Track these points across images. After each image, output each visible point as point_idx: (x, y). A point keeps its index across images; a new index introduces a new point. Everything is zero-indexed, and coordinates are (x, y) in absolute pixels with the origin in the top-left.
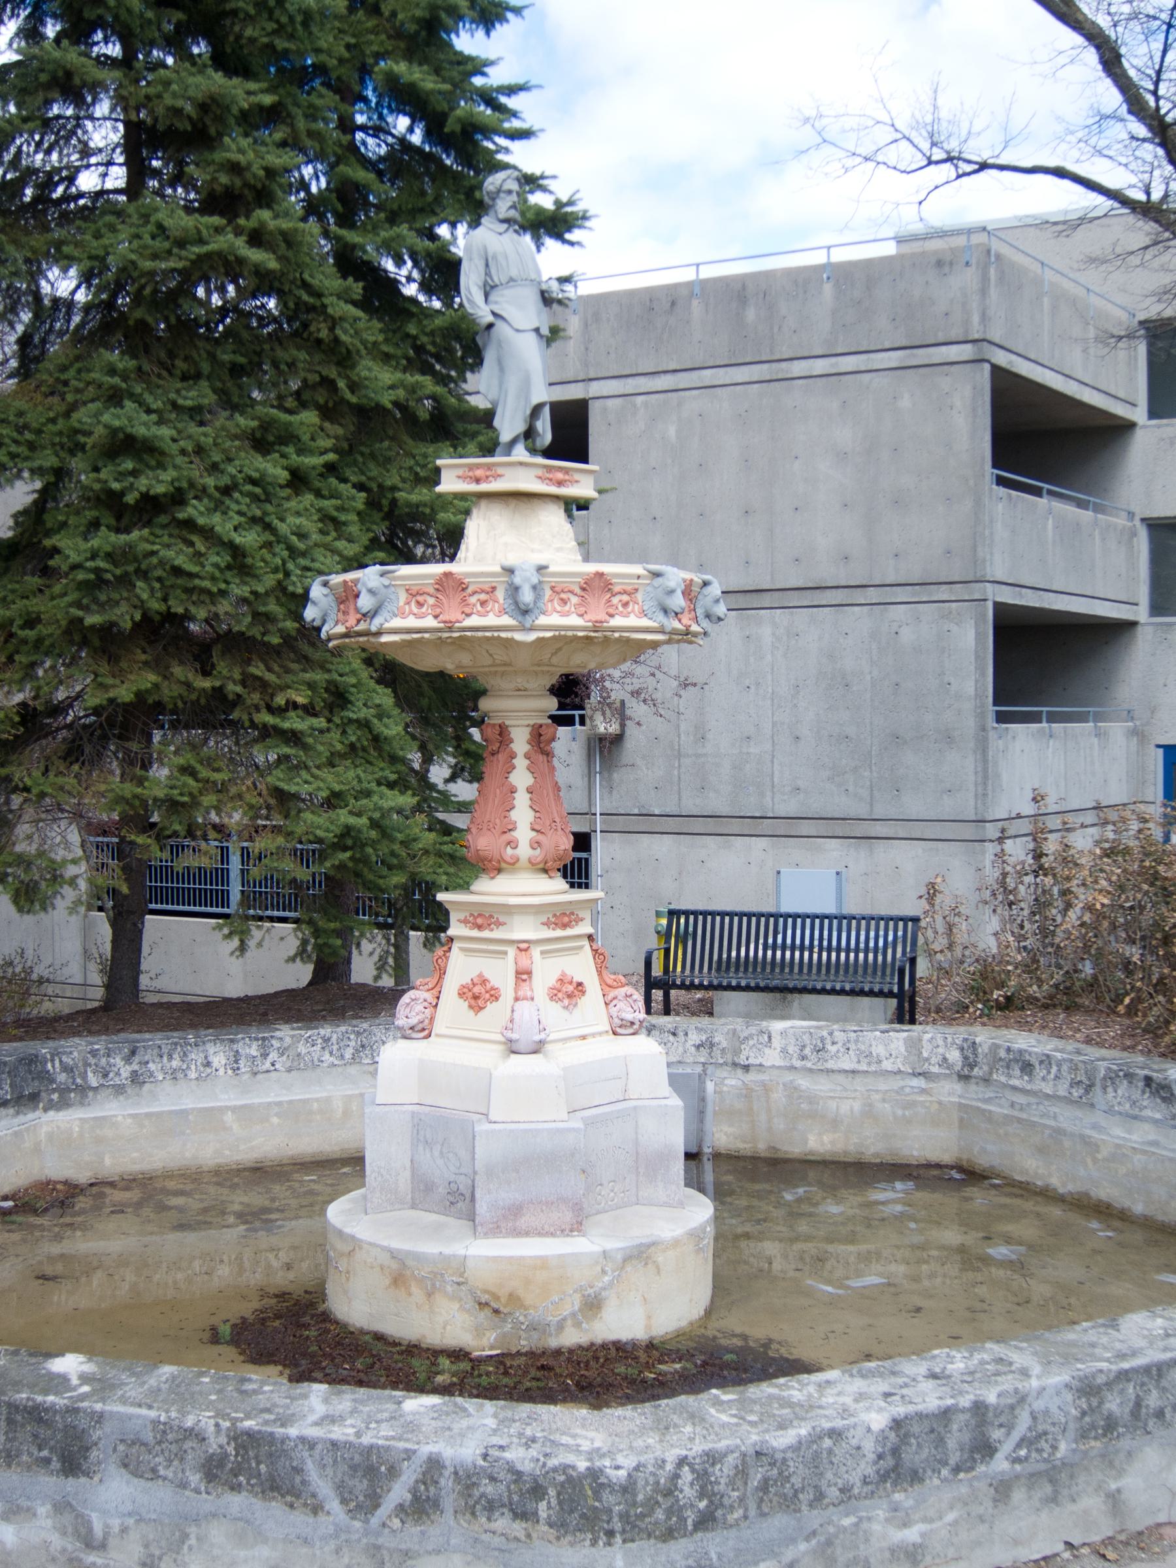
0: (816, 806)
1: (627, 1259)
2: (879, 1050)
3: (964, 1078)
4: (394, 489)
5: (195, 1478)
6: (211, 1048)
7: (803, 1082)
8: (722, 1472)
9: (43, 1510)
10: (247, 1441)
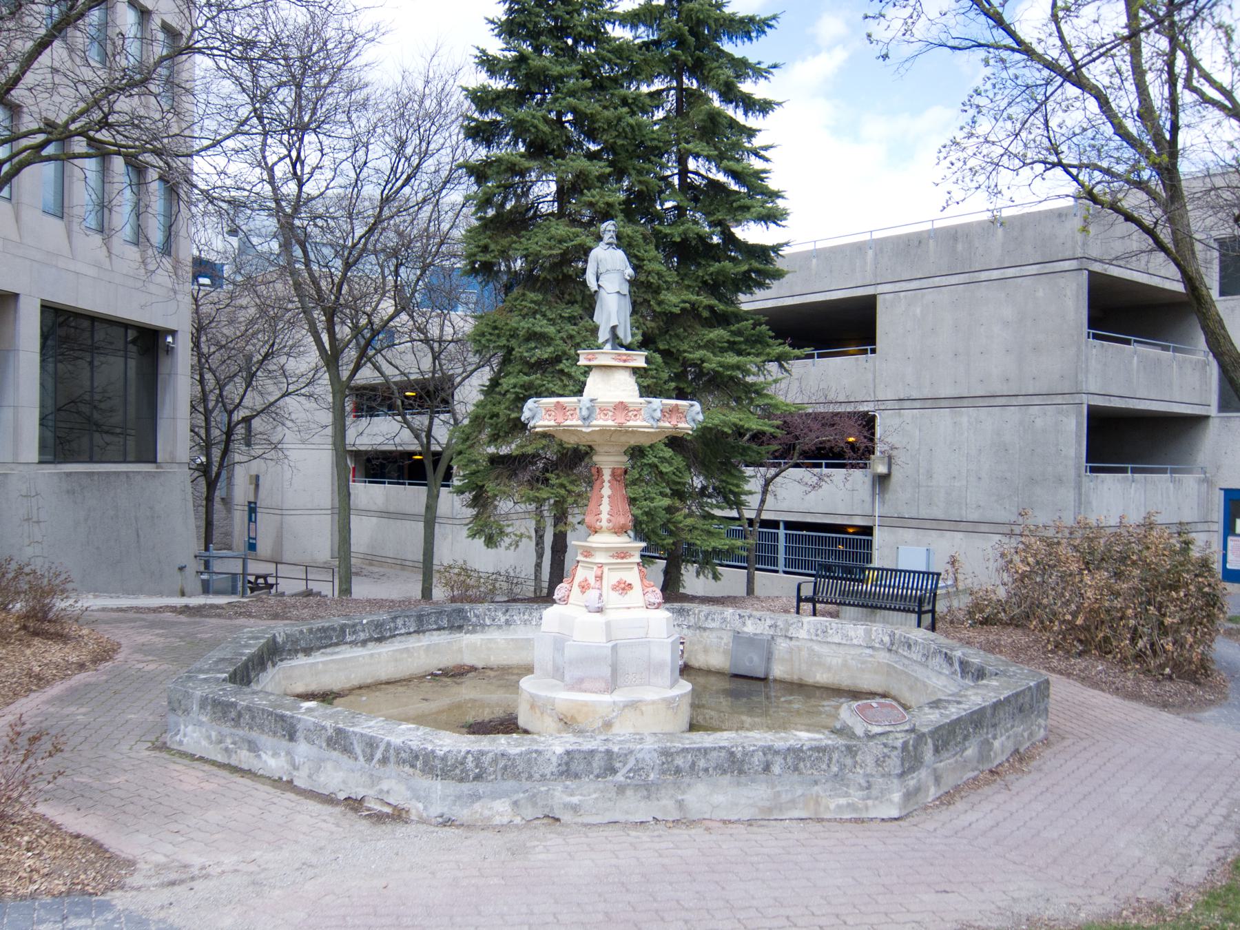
0: (990, 515)
1: (625, 706)
2: (851, 634)
3: (890, 650)
4: (685, 351)
5: (324, 745)
7: (816, 647)
8: (486, 760)
9: (283, 754)
10: (339, 731)
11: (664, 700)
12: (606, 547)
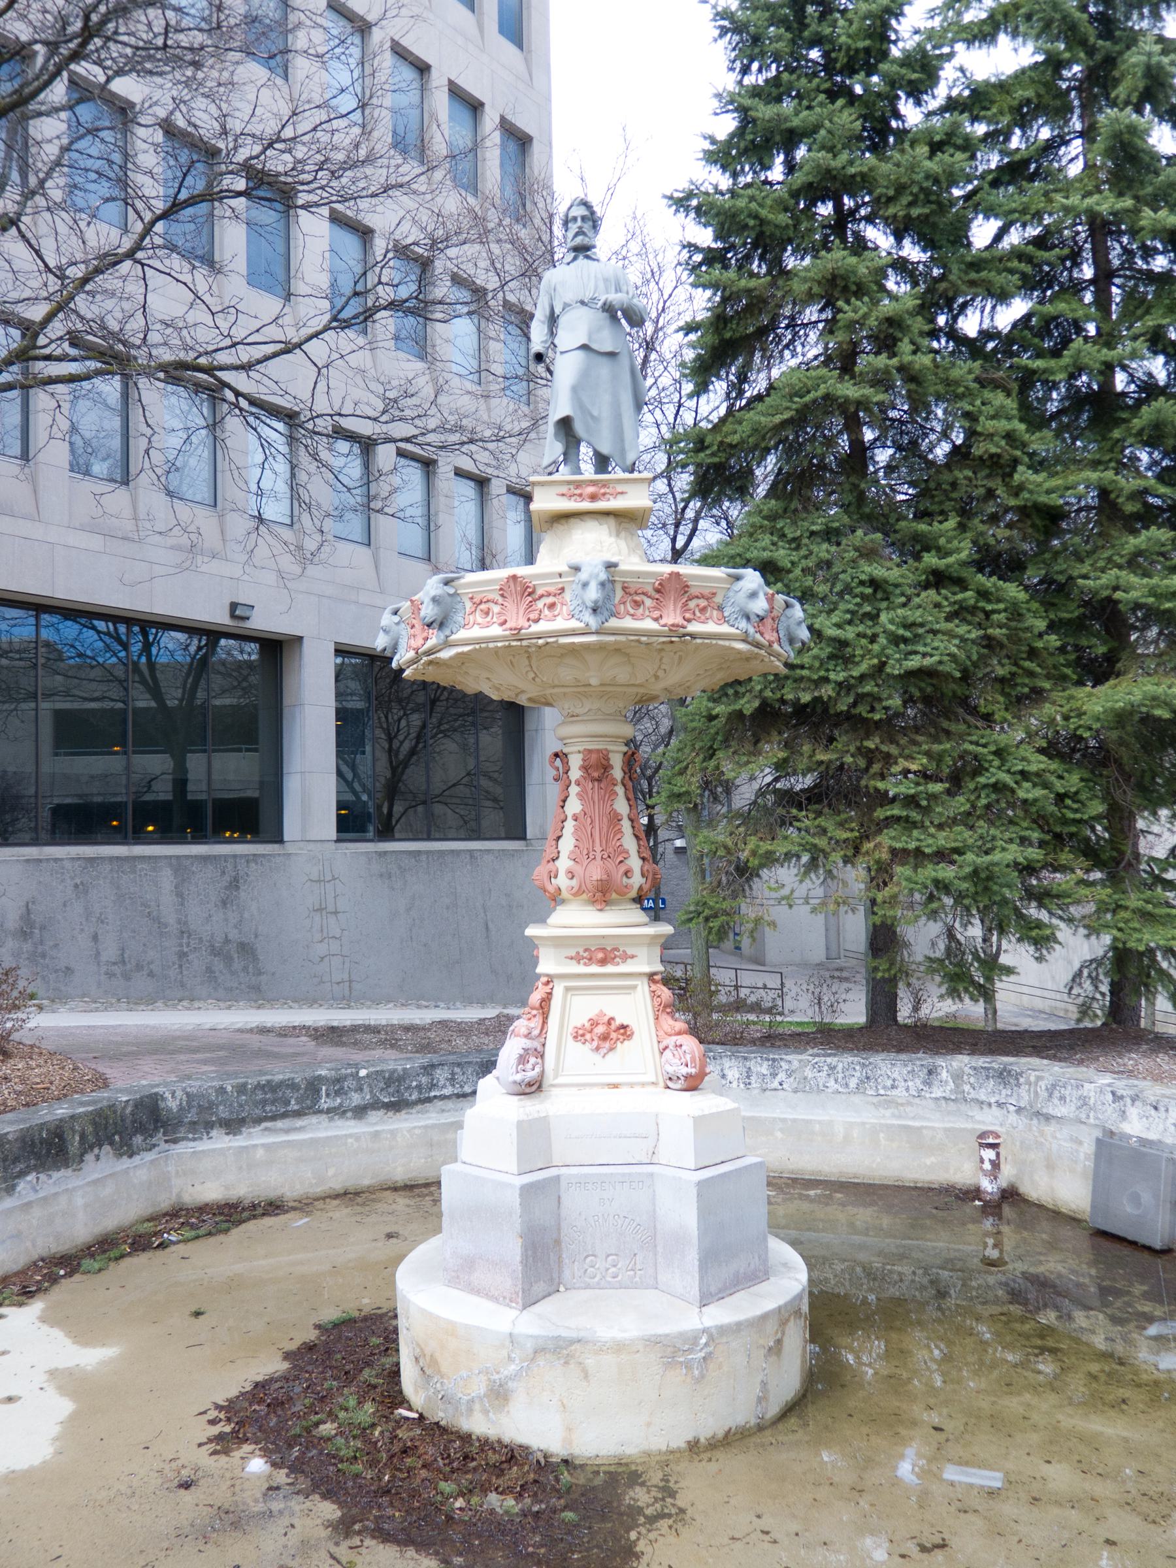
6: (727, 1063)
11: (654, 1342)
12: (585, 939)
